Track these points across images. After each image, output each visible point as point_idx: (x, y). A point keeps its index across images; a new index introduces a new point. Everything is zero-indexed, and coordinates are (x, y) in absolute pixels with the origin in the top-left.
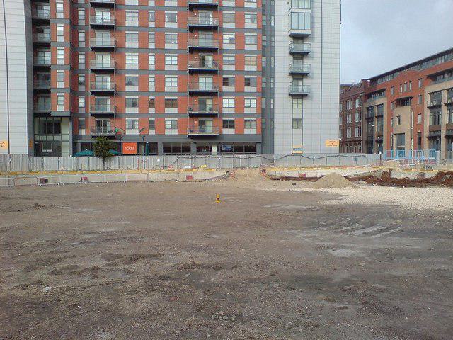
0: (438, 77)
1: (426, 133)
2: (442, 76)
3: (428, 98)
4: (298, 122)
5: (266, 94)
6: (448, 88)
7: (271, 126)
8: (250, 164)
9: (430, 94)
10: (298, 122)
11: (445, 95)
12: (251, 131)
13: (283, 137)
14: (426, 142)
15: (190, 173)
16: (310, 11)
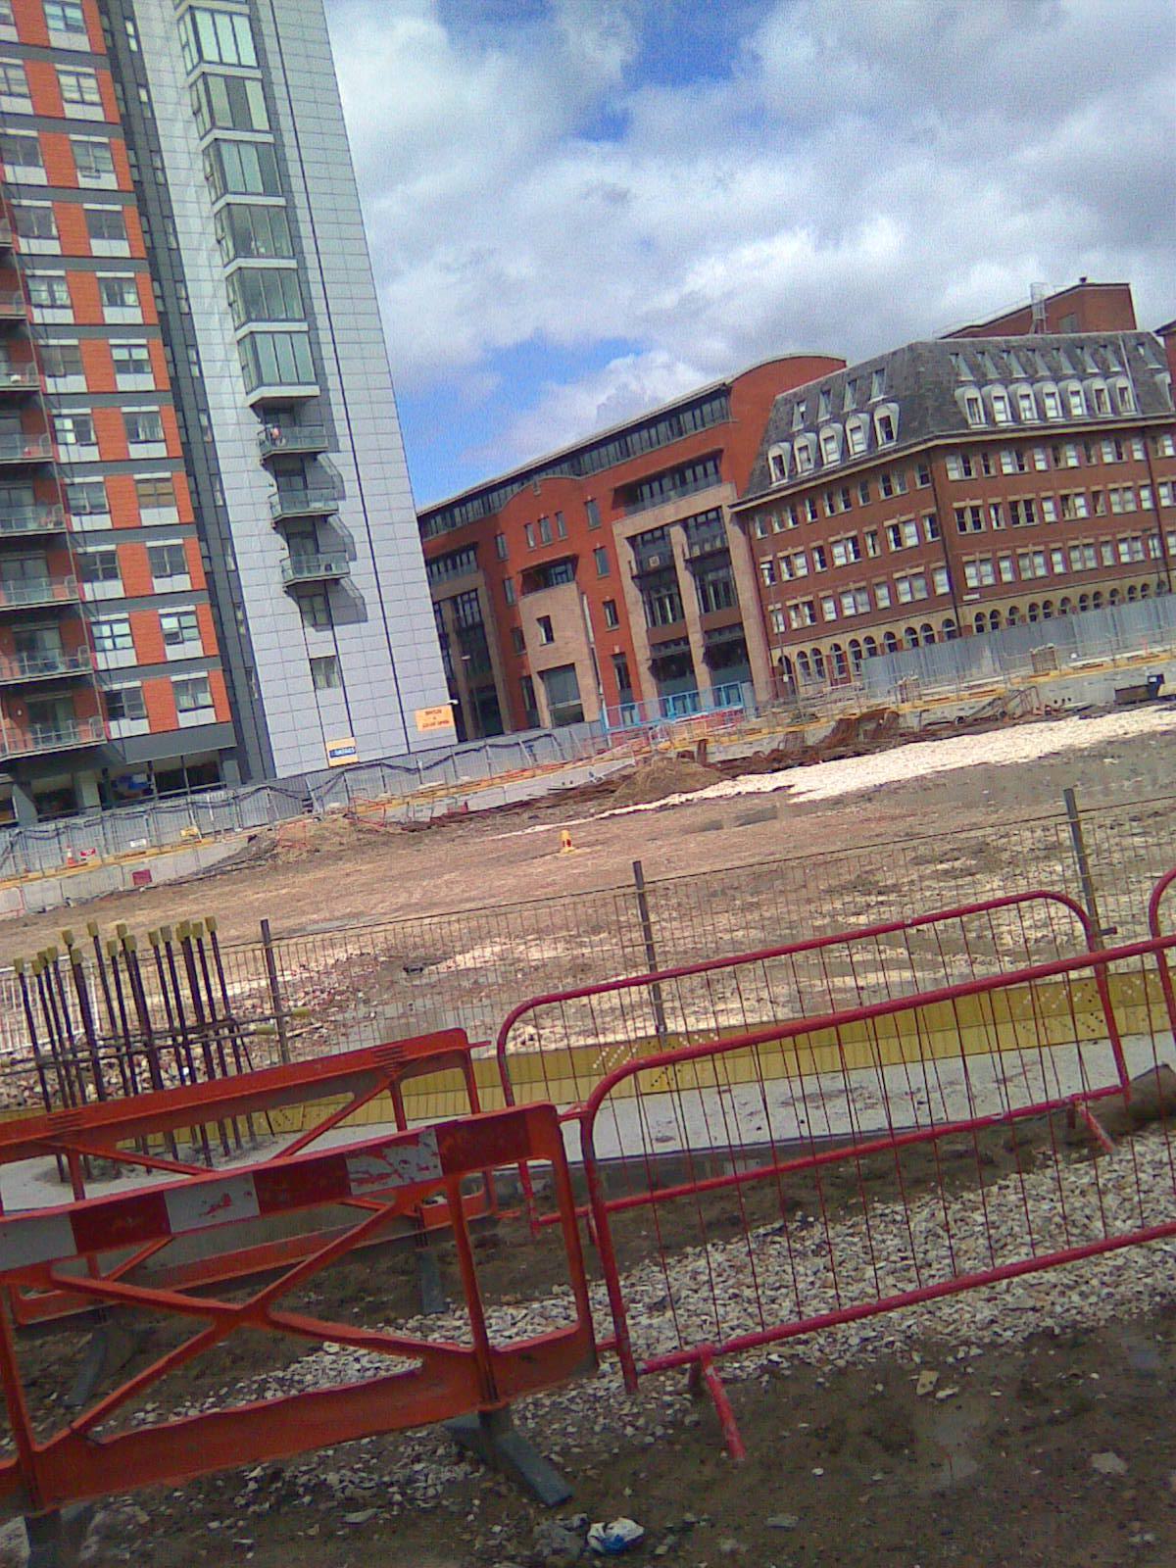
0: (646, 489)
1: (643, 655)
2: (699, 470)
3: (626, 555)
4: (324, 668)
5: (220, 596)
6: (682, 516)
7: (251, 694)
8: (240, 815)
9: (632, 540)
10: (324, 668)
11: (677, 535)
12: (201, 716)
13: (301, 733)
14: (647, 684)
15: (144, 864)
16: (304, 327)
